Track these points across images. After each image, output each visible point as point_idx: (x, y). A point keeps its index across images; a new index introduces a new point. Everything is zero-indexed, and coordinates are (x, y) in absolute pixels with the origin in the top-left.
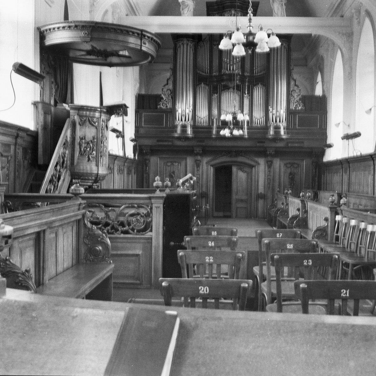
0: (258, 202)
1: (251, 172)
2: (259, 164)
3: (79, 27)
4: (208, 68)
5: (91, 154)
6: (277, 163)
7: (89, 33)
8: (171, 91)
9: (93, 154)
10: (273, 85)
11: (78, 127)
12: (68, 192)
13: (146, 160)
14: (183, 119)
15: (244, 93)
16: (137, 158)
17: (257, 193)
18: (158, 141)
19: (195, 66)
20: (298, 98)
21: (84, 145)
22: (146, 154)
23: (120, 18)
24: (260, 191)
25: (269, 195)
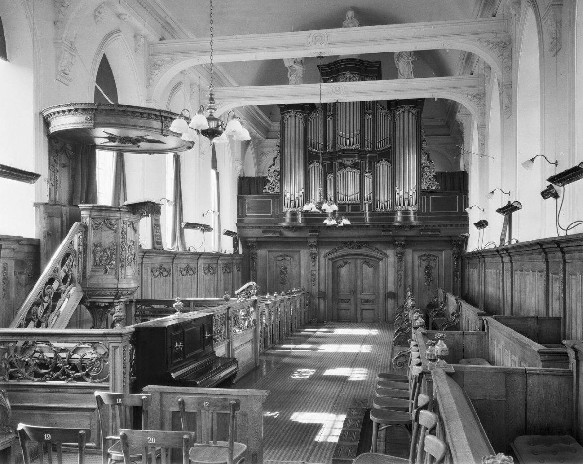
0: (387, 302)
1: (379, 266)
2: (387, 256)
3: (79, 111)
5: (109, 264)
6: (411, 255)
7: (92, 118)
8: (278, 172)
9: (112, 264)
10: (400, 161)
11: (91, 232)
13: (252, 254)
14: (292, 206)
15: (364, 172)
16: (241, 251)
17: (385, 292)
18: (264, 232)
19: (306, 142)
20: (432, 176)
21: (99, 254)
22: (252, 247)
24: (389, 290)
25: (401, 292)
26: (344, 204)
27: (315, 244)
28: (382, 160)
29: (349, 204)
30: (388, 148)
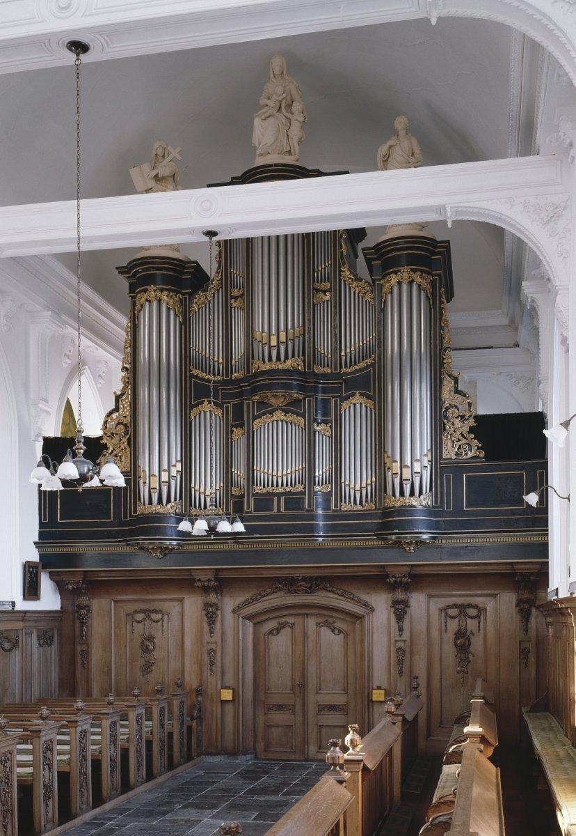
2: (372, 610)
4: (221, 361)
8: (126, 425)
12: (322, 708)
29: (279, 495)
30: (368, 366)
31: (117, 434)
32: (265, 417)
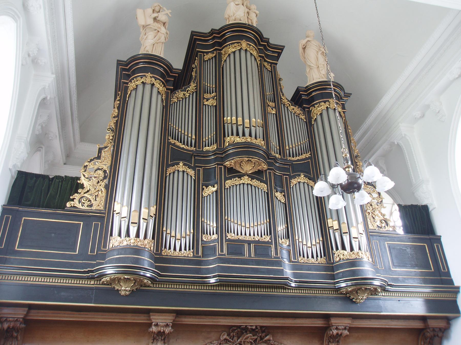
8: (105, 172)
19: (166, 131)
23: (109, 154)
26: (239, 240)
27: (167, 330)
28: (299, 175)
29: (249, 243)
30: (306, 159)
31: (95, 177)
32: (235, 179)
